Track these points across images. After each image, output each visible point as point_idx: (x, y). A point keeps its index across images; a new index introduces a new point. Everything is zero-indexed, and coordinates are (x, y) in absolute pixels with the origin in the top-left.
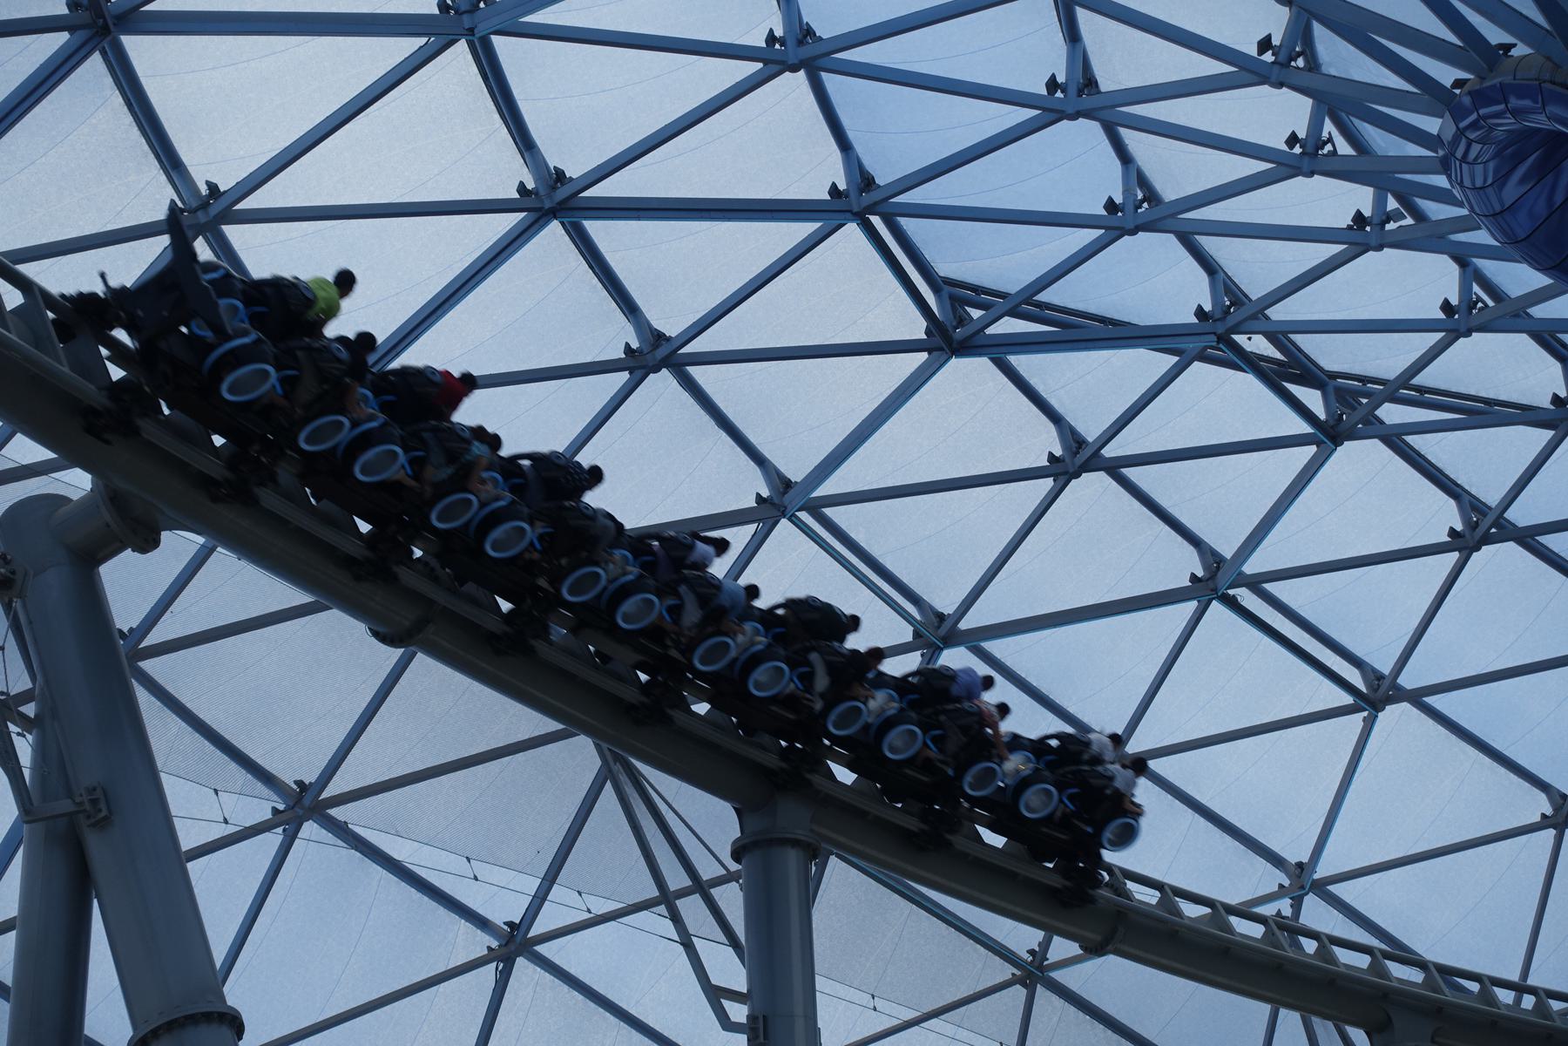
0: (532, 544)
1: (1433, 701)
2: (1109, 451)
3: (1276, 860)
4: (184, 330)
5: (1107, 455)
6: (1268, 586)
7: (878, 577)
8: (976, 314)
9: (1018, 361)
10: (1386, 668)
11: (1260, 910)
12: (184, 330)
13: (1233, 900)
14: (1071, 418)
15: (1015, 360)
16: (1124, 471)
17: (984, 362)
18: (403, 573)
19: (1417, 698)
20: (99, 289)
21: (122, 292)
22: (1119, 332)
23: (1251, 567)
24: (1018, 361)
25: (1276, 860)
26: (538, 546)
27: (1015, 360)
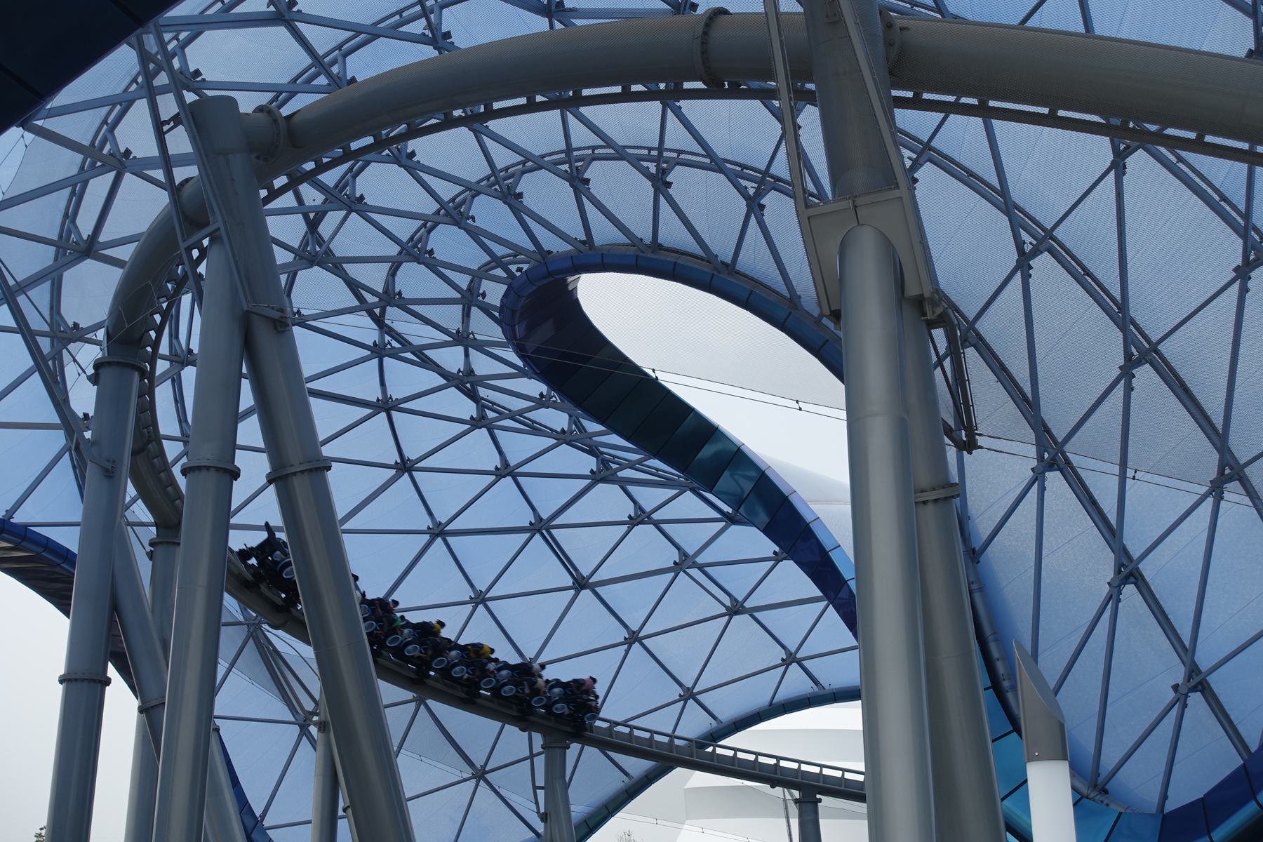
0: (376, 628)
1: (664, 526)
2: (655, 516)
3: (680, 684)
4: (270, 558)
5: (747, 607)
6: (706, 569)
7: (1227, 822)
8: (614, 466)
9: (631, 488)
10: (740, 599)
11: (629, 723)
12: (270, 558)
13: (619, 720)
14: (683, 545)
15: (756, 614)
16: (661, 525)
17: (616, 487)
18: (429, 682)
19: (751, 612)
20: (245, 548)
21: (252, 548)
22: (670, 482)
23: (700, 560)
24: (631, 488)
25: (680, 684)
26: (378, 628)
27: (756, 614)
